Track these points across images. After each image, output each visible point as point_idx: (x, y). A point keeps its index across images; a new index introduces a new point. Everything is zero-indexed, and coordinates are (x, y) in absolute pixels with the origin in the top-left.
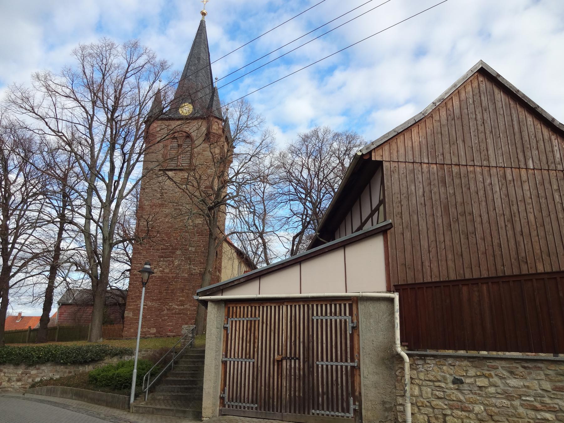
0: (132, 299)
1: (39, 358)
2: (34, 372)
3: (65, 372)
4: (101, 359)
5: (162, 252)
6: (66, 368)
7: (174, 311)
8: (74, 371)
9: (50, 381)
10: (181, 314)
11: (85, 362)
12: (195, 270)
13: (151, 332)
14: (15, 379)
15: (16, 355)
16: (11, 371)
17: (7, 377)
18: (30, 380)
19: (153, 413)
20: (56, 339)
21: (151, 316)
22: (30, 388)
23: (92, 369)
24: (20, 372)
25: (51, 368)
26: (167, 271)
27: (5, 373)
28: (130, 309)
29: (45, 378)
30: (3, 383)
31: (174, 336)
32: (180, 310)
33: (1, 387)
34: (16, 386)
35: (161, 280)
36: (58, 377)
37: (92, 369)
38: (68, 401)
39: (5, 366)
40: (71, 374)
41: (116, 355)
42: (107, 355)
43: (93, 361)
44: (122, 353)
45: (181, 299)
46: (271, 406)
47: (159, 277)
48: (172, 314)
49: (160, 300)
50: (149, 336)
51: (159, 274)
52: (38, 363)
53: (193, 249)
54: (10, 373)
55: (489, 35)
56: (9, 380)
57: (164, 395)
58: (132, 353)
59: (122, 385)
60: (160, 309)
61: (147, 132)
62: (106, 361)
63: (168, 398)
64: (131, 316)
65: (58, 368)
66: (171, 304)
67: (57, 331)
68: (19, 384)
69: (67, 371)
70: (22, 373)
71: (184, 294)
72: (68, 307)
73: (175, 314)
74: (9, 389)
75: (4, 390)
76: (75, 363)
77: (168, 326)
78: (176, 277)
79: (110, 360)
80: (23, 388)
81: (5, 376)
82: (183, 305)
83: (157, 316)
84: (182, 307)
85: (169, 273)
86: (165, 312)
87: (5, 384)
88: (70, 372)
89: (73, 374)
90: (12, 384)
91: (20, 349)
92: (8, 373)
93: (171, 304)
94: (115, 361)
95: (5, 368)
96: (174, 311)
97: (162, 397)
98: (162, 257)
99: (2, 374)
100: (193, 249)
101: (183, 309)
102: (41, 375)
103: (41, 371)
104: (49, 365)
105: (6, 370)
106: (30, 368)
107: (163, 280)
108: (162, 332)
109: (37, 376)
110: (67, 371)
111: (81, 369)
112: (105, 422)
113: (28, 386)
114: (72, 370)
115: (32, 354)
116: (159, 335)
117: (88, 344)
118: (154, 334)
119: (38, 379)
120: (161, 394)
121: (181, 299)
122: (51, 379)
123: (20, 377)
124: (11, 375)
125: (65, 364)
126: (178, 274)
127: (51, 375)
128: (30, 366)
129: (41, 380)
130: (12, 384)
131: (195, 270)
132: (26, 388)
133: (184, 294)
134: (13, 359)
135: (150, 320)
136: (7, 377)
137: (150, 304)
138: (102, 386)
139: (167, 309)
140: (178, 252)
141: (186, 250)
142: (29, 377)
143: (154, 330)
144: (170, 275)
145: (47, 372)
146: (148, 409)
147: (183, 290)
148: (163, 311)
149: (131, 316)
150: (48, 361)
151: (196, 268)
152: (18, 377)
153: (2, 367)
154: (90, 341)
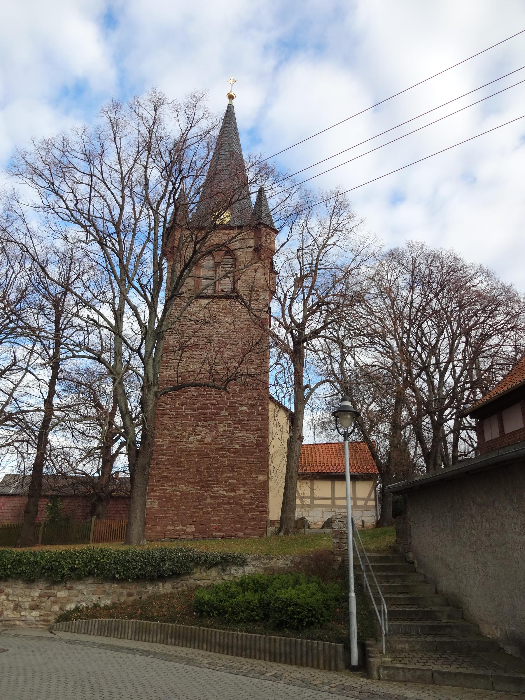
0: (158, 481)
1: (73, 569)
2: (62, 594)
3: (121, 594)
4: (188, 572)
5: (200, 413)
6: (122, 587)
7: (221, 500)
8: (139, 593)
9: (95, 611)
10: (232, 503)
11: (161, 577)
12: (249, 438)
13: (188, 530)
14: (27, 605)
15: (29, 563)
16: (19, 591)
17: (12, 601)
18: (56, 608)
19: (433, 681)
20: (40, 541)
21: (187, 506)
22: (58, 621)
23: (172, 590)
24: (37, 594)
25: (94, 587)
26: (208, 439)
27: (8, 595)
28: (154, 496)
29: (84, 604)
30: (6, 613)
31: (222, 537)
32: (230, 498)
33: (2, 618)
34: (29, 617)
35: (200, 454)
36: (108, 602)
37: (172, 590)
38: (173, 650)
39: (8, 583)
40: (132, 598)
41: (216, 564)
42: (197, 564)
43: (175, 575)
44: (226, 560)
45: (231, 481)
46: (197, 638)
47: (197, 449)
48: (219, 503)
49: (199, 482)
50: (184, 536)
51: (196, 445)
52: (70, 578)
53: (245, 409)
54: (17, 596)
55: (475, 180)
56: (17, 607)
57: (409, 642)
58: (244, 562)
59: (301, 621)
60: (199, 497)
61: (139, 260)
62: (197, 575)
63: (417, 647)
64: (156, 507)
65: (107, 586)
66: (215, 489)
67: (41, 528)
68: (36, 613)
69: (125, 592)
70: (40, 596)
71: (236, 474)
72: (10, 499)
73: (223, 503)
74: (17, 623)
75: (8, 624)
76: (141, 578)
77: (214, 521)
78: (221, 450)
79: (204, 574)
80: (44, 621)
81: (8, 600)
82: (233, 490)
83: (195, 506)
84: (233, 494)
85: (210, 444)
86: (208, 501)
87: (9, 614)
88: (130, 595)
89: (136, 597)
90: (22, 614)
91: (34, 554)
92: (14, 595)
93: (215, 489)
94: (212, 577)
95: (7, 587)
96: (221, 500)
97: (407, 646)
98: (200, 420)
99: (4, 597)
100: (245, 409)
101: (234, 497)
102: (76, 599)
103: (74, 592)
104: (90, 581)
105: (10, 591)
106: (56, 587)
107: (203, 453)
108: (205, 530)
109: (69, 601)
110: (125, 592)
111: (150, 589)
112: (341, 697)
113: (52, 618)
114: (134, 591)
115: (60, 564)
116: (200, 536)
117: (125, 548)
118: (192, 533)
119: (71, 606)
120: (404, 639)
121: (231, 481)
122: (96, 606)
123: (37, 603)
124: (20, 599)
125: (123, 580)
126: (225, 444)
127: (95, 598)
128: (55, 583)
129: (77, 608)
130: (22, 614)
131: (249, 438)
132: (48, 621)
133: (236, 474)
134: (24, 572)
135: (185, 514)
136: (12, 601)
137: (185, 488)
138: (239, 622)
139: (211, 497)
140: (224, 413)
141: (234, 410)
142: (54, 603)
143: (191, 528)
144: (213, 447)
145: (86, 594)
146: (418, 673)
147: (233, 469)
148: (204, 499)
149: (156, 507)
150: (90, 574)
151: (250, 436)
152: (32, 603)
153: (1, 586)
154: (128, 541)
